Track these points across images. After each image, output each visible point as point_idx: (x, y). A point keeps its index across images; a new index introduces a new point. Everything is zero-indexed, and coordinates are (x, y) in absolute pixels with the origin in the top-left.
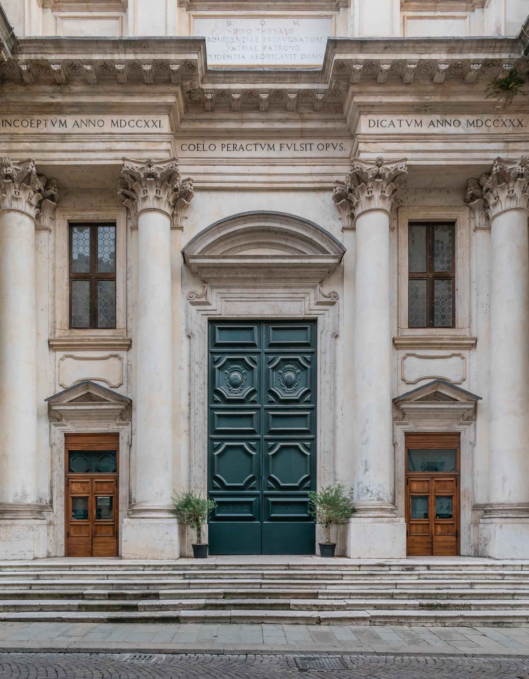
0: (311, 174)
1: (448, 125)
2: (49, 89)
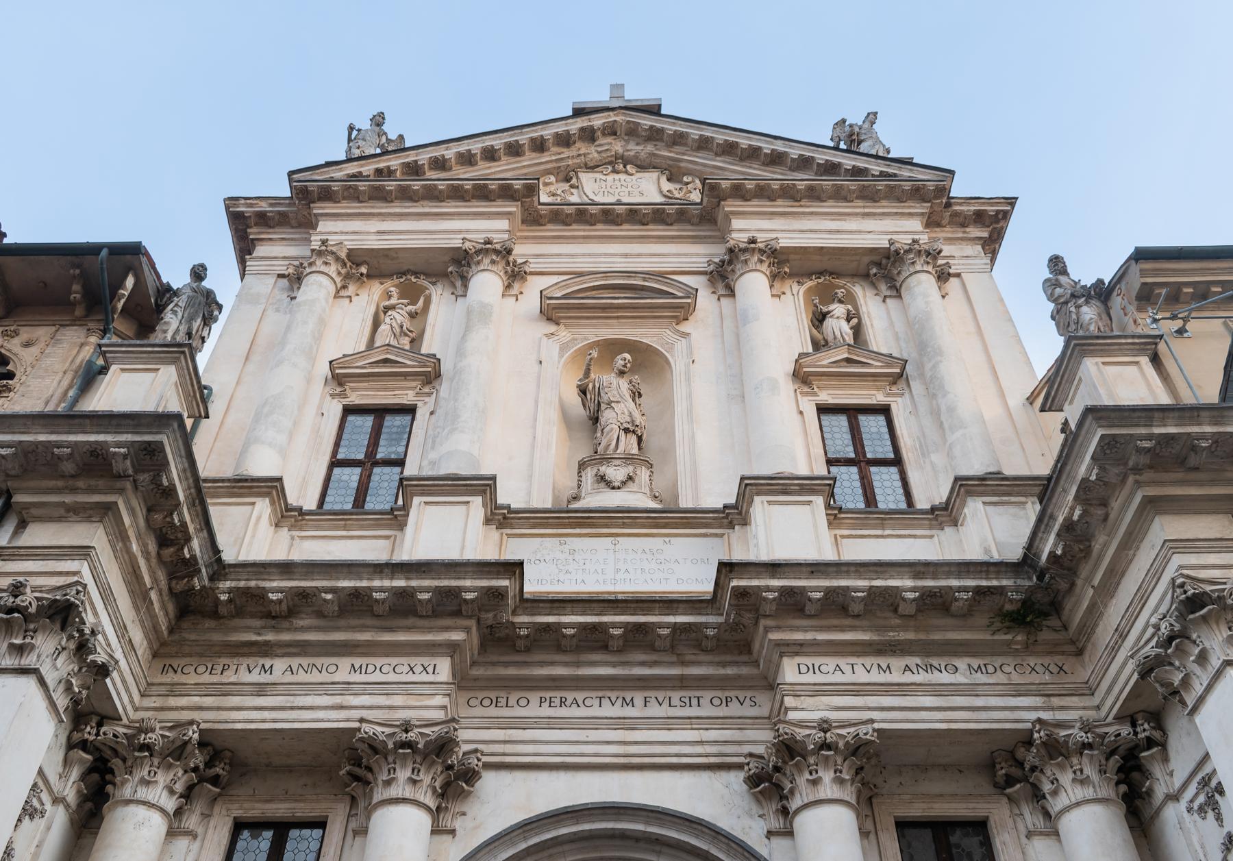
0: (701, 743)
1: (936, 672)
2: (258, 623)
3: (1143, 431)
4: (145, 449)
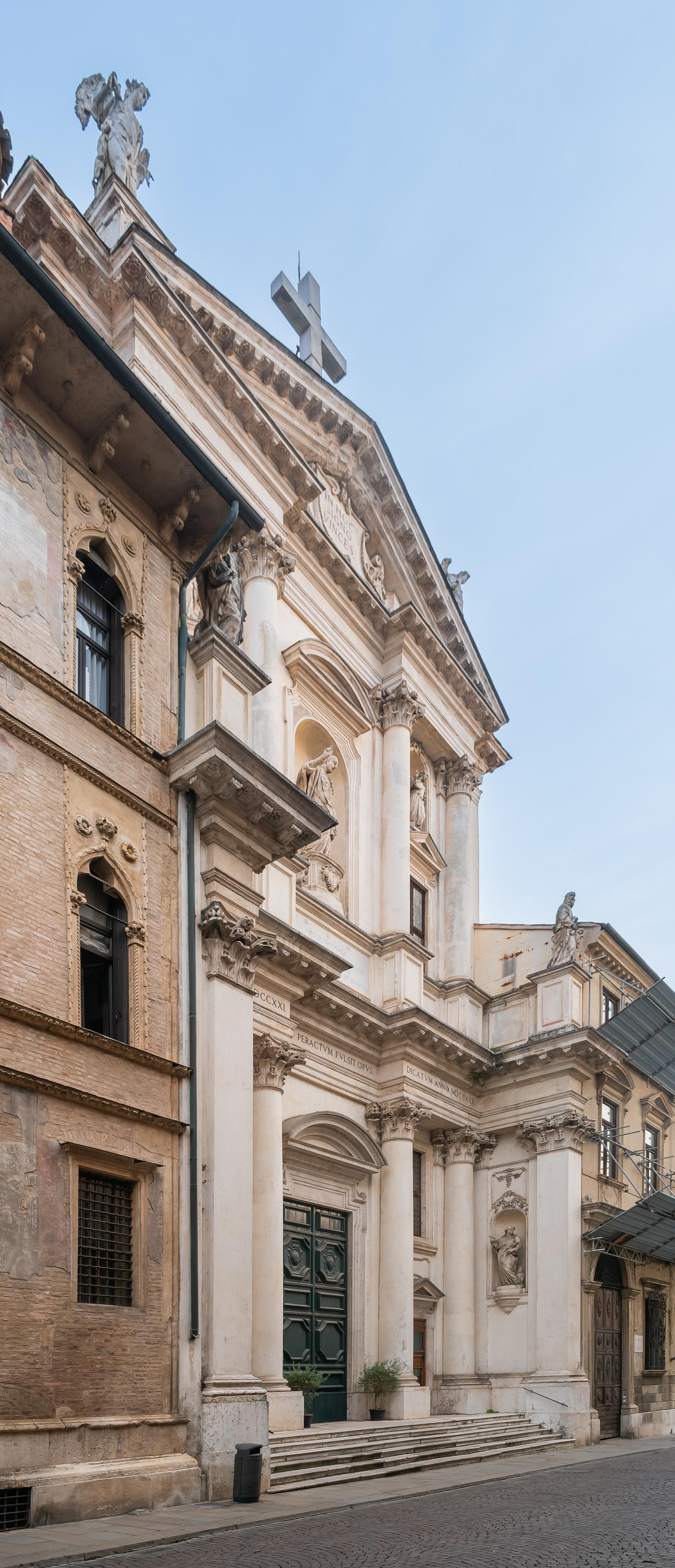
0: (355, 1087)
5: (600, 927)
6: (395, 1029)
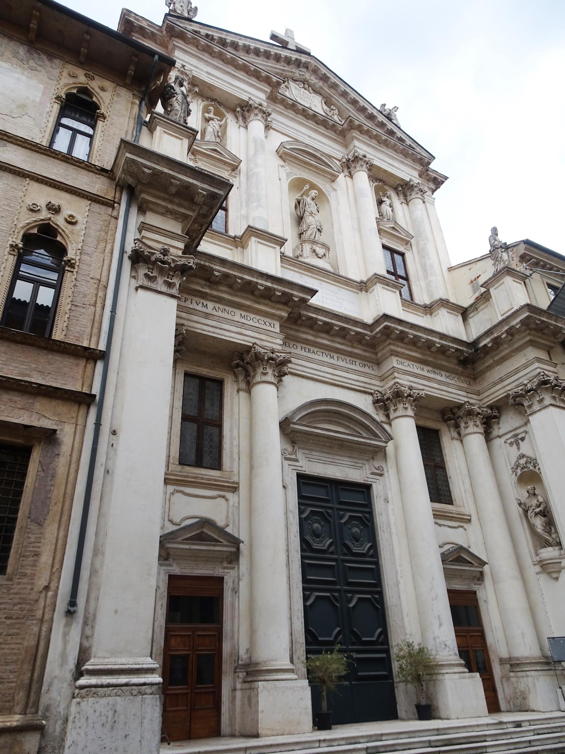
2: (203, 282)
3: (538, 317)
4: (213, 196)
5: (523, 243)
6: (377, 333)
